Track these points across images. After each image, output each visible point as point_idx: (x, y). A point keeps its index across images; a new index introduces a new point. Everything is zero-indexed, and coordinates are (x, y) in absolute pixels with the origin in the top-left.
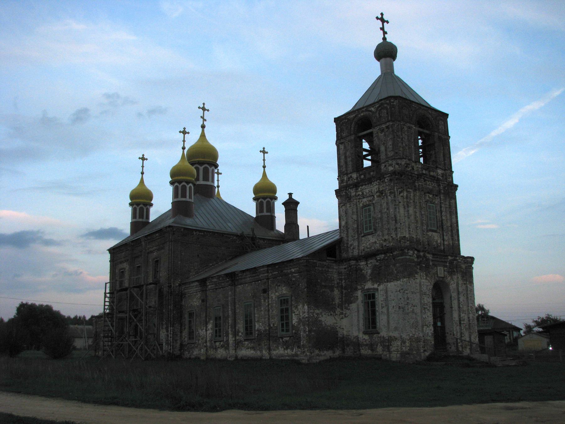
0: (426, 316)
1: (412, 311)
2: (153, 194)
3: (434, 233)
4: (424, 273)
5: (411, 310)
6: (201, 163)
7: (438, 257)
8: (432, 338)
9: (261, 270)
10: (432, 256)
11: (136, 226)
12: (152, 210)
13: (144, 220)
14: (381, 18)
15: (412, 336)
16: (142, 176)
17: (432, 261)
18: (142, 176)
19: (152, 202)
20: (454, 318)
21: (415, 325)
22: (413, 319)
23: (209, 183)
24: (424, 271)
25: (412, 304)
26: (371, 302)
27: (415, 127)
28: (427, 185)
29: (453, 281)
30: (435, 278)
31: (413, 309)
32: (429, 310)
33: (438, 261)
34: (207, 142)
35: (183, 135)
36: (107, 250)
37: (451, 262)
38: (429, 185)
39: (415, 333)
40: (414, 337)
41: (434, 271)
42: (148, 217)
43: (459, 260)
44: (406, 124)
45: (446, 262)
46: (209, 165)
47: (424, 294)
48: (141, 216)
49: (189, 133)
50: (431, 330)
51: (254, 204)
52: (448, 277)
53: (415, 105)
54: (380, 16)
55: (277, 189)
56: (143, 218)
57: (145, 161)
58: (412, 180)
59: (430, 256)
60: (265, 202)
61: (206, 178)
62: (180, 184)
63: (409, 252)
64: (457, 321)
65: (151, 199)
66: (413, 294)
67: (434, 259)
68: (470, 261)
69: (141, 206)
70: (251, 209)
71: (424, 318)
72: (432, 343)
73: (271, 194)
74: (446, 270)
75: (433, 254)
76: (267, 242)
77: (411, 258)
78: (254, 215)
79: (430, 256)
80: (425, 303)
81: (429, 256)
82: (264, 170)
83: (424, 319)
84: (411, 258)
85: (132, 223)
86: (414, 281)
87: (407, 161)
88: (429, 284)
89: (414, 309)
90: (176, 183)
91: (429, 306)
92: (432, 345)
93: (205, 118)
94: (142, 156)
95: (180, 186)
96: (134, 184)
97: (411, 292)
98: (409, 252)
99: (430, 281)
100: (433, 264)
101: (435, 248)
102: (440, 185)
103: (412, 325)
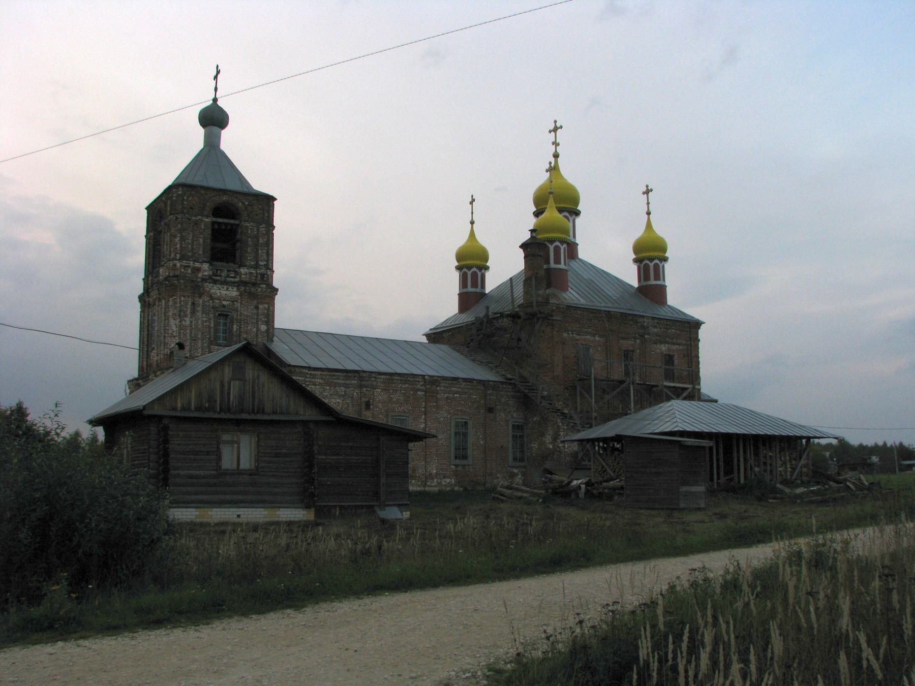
2: (667, 242)
9: (396, 378)
11: (467, 300)
12: (488, 276)
13: (478, 290)
16: (649, 218)
18: (649, 218)
36: (423, 335)
42: (483, 286)
48: (475, 285)
51: (634, 268)
55: (668, 246)
56: (477, 287)
60: (469, 273)
62: (651, 262)
65: (487, 260)
69: (474, 269)
70: (630, 276)
73: (660, 254)
78: (636, 284)
82: (472, 227)
85: (461, 295)
96: (461, 240)
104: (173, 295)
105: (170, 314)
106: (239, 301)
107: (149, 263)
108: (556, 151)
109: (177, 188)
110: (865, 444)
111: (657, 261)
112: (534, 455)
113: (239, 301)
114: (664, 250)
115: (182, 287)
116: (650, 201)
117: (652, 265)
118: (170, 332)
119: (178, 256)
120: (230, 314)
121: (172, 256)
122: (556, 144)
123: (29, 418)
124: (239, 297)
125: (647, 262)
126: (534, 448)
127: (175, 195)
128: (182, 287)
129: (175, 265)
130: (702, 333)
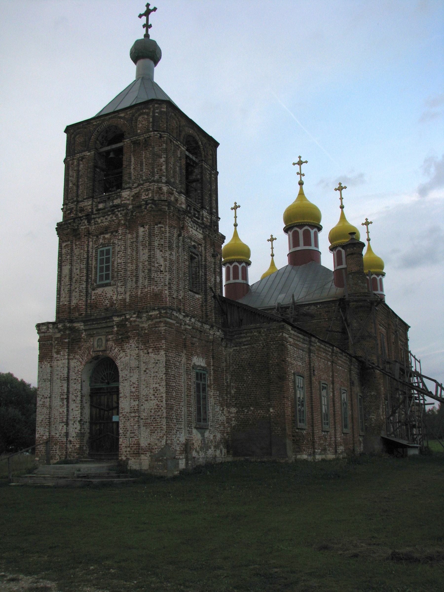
0: (63, 410)
1: (43, 404)
3: (106, 289)
4: (65, 351)
5: (41, 403)
6: (301, 226)
7: (94, 323)
8: (76, 439)
10: (82, 324)
14: (150, 9)
15: (39, 438)
16: (272, 259)
17: (85, 330)
19: (384, 271)
20: (122, 408)
21: (46, 423)
22: (43, 414)
23: (313, 247)
24: (67, 349)
25: (43, 396)
26: (202, 384)
27: (89, 152)
28: (98, 224)
29: (124, 353)
30: (89, 353)
31: (44, 402)
32: (74, 400)
33: (96, 329)
34: (306, 200)
35: (339, 192)
37: (121, 325)
38: (103, 222)
39: (45, 433)
40: (42, 438)
41: (88, 344)
43: (131, 319)
44: (74, 158)
45: (112, 327)
46: (310, 227)
47: (63, 380)
49: (335, 190)
50: (76, 428)
52: (113, 348)
53: (96, 122)
54: (151, 8)
57: (370, 226)
58: (69, 229)
59: (80, 326)
61: (307, 242)
62: (231, 265)
63: (41, 328)
64: (127, 413)
66: (45, 381)
67: (87, 327)
68: (157, 314)
71: (61, 412)
72: (76, 447)
73: (377, 270)
74: (112, 338)
75: (84, 322)
76: (320, 306)
77: (46, 335)
79: (80, 326)
80: (64, 393)
81: (79, 325)
82: (235, 229)
83: (61, 413)
84: (46, 334)
86: (49, 364)
87: (71, 205)
88: (79, 363)
89: (46, 401)
90: (244, 263)
91: (75, 394)
92: (75, 450)
93: (302, 173)
94: (370, 222)
95: (231, 267)
97: (44, 379)
98: (41, 328)
99: (81, 359)
100: (87, 335)
101: (107, 309)
102: (117, 215)
103: (41, 423)
104: (160, 223)
105: (156, 244)
106: (203, 245)
107: (210, 183)
108: (301, 180)
109: (159, 104)
110: (16, 375)
111: (244, 264)
112: (373, 425)
113: (203, 245)
114: (382, 267)
115: (171, 214)
116: (369, 231)
117: (240, 267)
118: (156, 265)
119: (164, 179)
120: (197, 257)
121: (157, 177)
122: (300, 174)
123: (32, 387)
124: (203, 242)
125: (237, 264)
126: (373, 419)
127: (157, 111)
128: (171, 214)
129: (160, 189)
130: (410, 329)
